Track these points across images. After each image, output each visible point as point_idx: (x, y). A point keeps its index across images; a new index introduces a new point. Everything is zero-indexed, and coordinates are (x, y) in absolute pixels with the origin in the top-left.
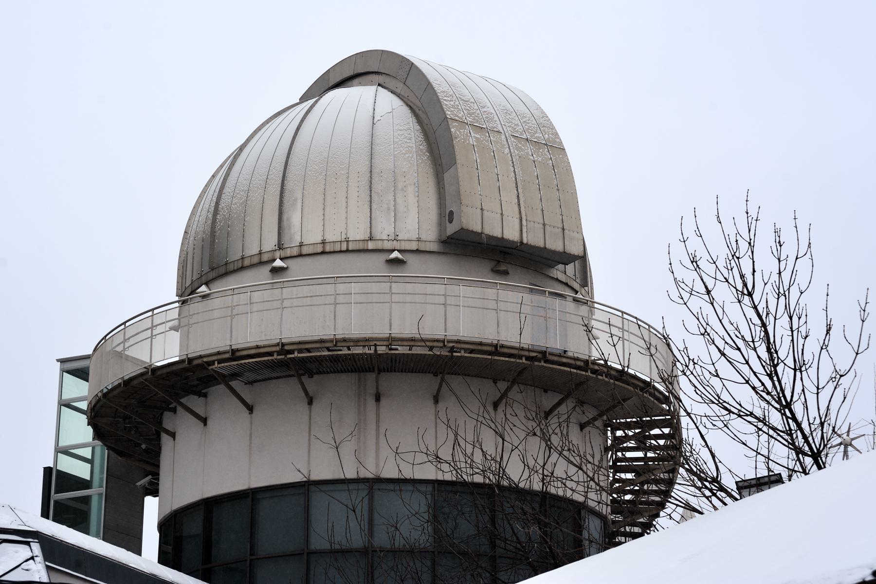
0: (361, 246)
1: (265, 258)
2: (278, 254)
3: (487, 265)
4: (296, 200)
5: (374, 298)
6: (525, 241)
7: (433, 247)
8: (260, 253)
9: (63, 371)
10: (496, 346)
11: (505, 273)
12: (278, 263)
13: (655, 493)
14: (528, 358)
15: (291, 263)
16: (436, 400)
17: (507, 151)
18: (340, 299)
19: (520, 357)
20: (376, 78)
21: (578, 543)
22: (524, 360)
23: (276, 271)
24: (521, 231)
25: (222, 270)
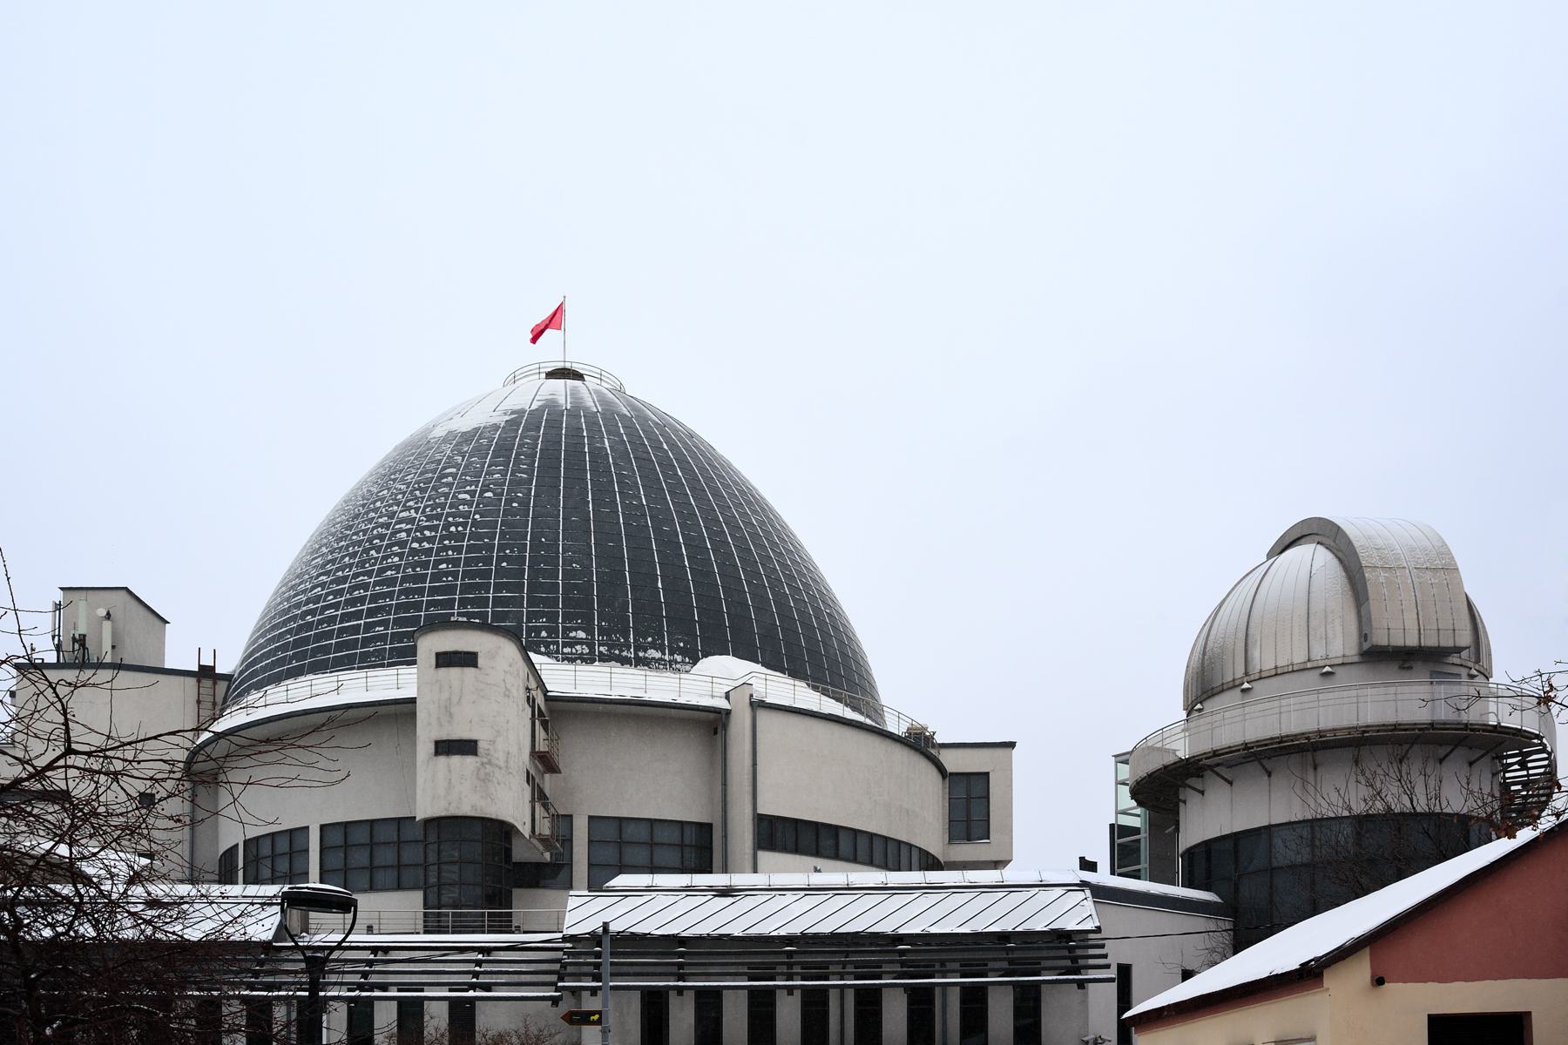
0: (1302, 667)
1: (1237, 683)
2: (1245, 679)
3: (1394, 667)
4: (1256, 641)
5: (1307, 706)
6: (1423, 645)
7: (1356, 659)
8: (1234, 680)
9: (1117, 762)
10: (1395, 725)
11: (1410, 668)
12: (1246, 685)
13: (1543, 795)
14: (1420, 729)
15: (1254, 684)
16: (1357, 762)
17: (1410, 581)
18: (1283, 709)
19: (1414, 729)
20: (1318, 538)
21: (1468, 843)
22: (1417, 731)
23: (1244, 691)
24: (1420, 638)
25: (1210, 693)
